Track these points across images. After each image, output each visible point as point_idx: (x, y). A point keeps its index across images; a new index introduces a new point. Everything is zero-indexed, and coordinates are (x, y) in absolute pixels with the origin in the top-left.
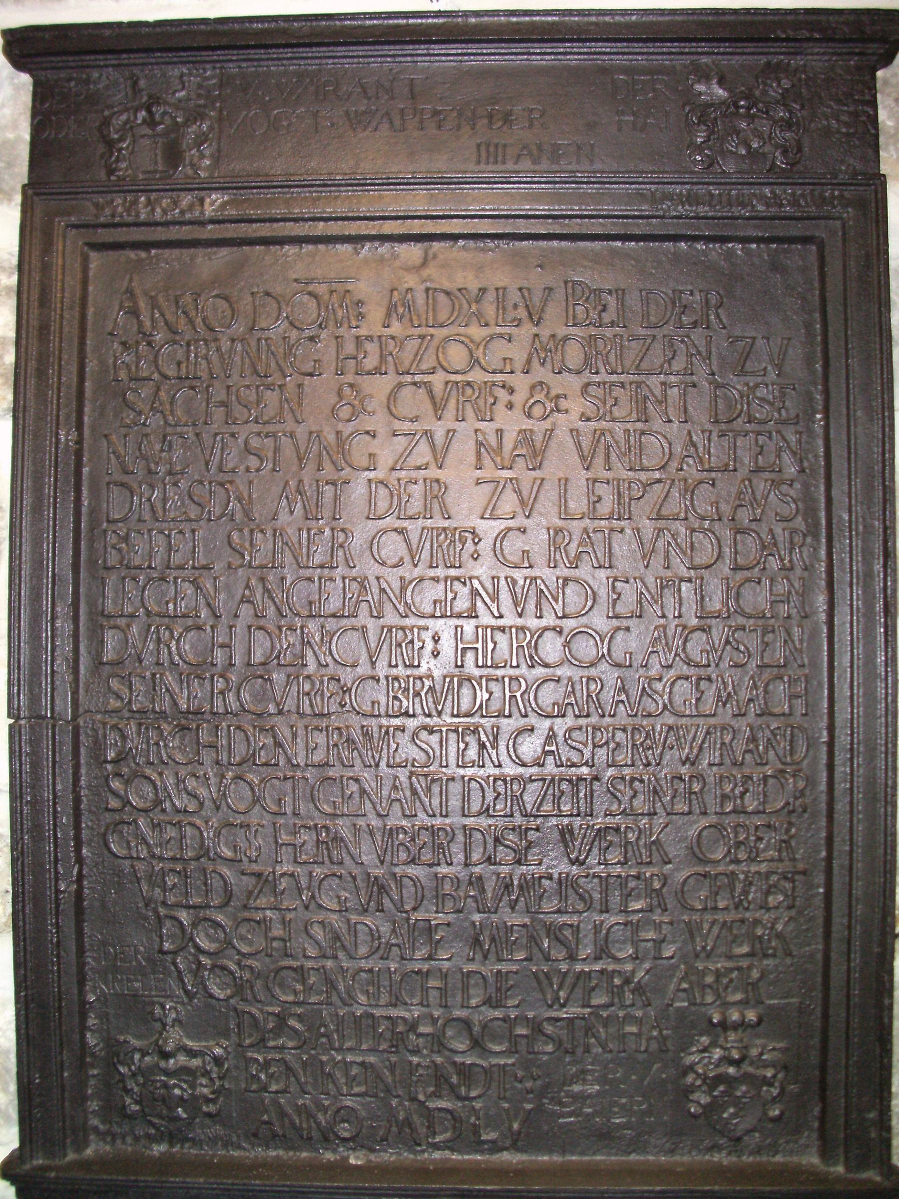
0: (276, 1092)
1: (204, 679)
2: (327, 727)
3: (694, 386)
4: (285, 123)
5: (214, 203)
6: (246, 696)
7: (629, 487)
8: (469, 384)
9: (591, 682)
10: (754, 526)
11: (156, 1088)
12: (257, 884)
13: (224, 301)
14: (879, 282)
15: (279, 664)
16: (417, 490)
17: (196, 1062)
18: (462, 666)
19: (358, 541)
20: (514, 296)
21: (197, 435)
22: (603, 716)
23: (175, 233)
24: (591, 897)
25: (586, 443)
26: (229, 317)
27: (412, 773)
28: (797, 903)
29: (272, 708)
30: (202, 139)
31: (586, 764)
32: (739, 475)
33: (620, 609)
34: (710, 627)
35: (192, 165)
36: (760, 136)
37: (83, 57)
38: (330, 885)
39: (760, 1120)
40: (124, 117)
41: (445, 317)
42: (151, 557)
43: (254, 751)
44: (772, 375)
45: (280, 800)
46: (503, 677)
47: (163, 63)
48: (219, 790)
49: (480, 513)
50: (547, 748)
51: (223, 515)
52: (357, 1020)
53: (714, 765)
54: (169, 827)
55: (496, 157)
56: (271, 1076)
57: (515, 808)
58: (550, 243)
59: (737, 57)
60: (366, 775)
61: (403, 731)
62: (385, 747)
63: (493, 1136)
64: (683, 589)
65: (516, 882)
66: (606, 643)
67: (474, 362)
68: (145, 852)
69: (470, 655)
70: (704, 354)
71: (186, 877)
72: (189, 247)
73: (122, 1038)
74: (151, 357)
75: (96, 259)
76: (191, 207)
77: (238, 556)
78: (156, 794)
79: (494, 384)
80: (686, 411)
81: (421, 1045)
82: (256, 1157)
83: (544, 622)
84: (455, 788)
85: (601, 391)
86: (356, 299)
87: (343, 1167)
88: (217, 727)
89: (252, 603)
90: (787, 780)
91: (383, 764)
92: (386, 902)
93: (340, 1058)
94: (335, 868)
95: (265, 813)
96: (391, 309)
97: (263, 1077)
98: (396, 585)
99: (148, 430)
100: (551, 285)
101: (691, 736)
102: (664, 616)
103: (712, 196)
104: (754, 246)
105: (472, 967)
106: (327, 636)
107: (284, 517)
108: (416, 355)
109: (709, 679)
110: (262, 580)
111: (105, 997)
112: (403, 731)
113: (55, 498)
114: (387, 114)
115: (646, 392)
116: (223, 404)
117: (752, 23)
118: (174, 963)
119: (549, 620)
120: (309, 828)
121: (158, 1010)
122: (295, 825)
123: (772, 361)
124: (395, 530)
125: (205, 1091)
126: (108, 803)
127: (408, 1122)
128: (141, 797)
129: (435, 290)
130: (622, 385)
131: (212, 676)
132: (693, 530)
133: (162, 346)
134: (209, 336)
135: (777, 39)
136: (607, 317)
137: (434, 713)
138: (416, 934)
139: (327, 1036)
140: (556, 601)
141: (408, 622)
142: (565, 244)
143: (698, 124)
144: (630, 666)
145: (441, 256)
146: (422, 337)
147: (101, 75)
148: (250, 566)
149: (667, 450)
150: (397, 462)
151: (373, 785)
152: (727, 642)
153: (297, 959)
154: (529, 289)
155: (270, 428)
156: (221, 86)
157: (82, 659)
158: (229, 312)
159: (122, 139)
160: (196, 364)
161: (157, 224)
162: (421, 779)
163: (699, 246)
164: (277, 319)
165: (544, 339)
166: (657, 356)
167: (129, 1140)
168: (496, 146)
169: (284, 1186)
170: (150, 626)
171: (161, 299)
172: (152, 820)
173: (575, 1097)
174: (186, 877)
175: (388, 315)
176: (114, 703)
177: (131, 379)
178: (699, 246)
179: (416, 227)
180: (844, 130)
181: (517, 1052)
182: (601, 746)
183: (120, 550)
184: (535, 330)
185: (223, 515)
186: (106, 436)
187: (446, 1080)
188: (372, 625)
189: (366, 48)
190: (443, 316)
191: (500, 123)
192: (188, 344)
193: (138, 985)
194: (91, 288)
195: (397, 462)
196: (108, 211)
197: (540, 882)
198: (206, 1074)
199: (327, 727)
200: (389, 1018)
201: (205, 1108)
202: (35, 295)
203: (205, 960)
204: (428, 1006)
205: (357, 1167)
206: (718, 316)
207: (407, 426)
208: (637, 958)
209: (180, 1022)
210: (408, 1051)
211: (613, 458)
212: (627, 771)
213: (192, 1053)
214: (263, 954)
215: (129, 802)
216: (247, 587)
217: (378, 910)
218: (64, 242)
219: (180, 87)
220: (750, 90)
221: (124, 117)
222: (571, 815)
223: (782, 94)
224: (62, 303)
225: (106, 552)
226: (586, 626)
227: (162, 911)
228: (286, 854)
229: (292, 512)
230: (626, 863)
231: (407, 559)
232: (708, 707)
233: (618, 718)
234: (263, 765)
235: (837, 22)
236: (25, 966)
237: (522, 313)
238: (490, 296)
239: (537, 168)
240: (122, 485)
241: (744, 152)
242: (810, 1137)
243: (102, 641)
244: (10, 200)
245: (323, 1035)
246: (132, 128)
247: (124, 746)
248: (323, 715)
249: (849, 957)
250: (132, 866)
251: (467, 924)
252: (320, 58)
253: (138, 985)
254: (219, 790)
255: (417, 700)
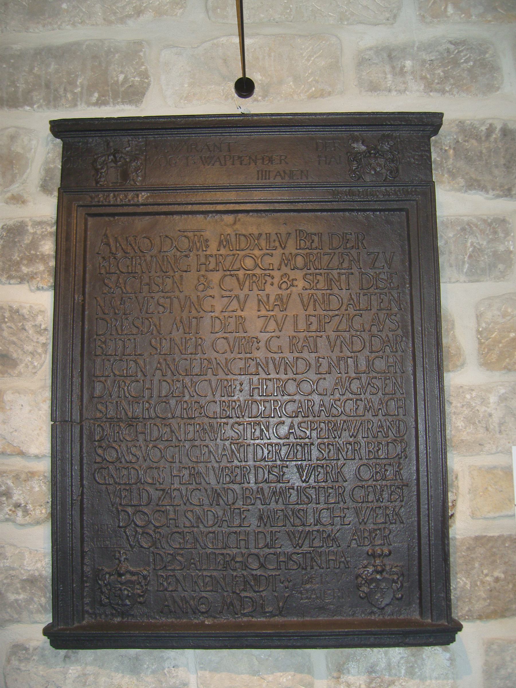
0: (172, 591)
1: (139, 403)
2: (194, 423)
3: (352, 274)
4: (174, 162)
5: (143, 197)
6: (158, 409)
7: (324, 318)
8: (254, 275)
9: (309, 402)
10: (379, 333)
11: (116, 591)
12: (163, 494)
13: (147, 240)
14: (433, 227)
15: (173, 396)
16: (232, 321)
17: (134, 578)
18: (253, 396)
19: (207, 344)
20: (274, 237)
21: (136, 297)
22: (315, 417)
23: (126, 210)
24: (312, 497)
25: (305, 300)
26: (150, 246)
27: (231, 443)
28: (405, 499)
29: (170, 415)
30: (136, 170)
31: (308, 438)
32: (373, 312)
33: (321, 370)
34: (361, 378)
35: (133, 180)
36: (380, 166)
37: (86, 133)
38: (196, 494)
39: (392, 599)
40: (103, 158)
41: (244, 246)
42: (116, 351)
43: (162, 435)
44: (386, 269)
45: (173, 456)
46: (271, 401)
47: (120, 136)
48: (146, 452)
49: (260, 330)
50: (291, 431)
51: (148, 332)
52: (208, 556)
53: (364, 437)
54: (123, 469)
55: (266, 176)
56: (169, 584)
57: (277, 457)
58: (289, 214)
59: (370, 132)
60: (212, 444)
61: (227, 424)
62: (219, 431)
63: (270, 609)
64: (349, 361)
65: (278, 490)
66: (315, 385)
67: (257, 265)
68: (112, 481)
69: (256, 391)
70: (357, 260)
71: (131, 492)
72: (133, 216)
73: (100, 568)
74: (116, 264)
75: (91, 221)
76: (133, 198)
77: (154, 350)
78: (118, 455)
79: (265, 275)
80: (349, 285)
81: (237, 567)
82: (162, 622)
83: (287, 377)
84: (251, 449)
85: (311, 277)
86: (205, 238)
87: (202, 625)
88: (145, 424)
89: (161, 370)
90: (397, 444)
91: (218, 440)
92: (221, 502)
93: (200, 574)
94: (198, 486)
95: (166, 462)
96: (220, 243)
97: (166, 584)
98: (224, 361)
99: (115, 295)
100: (290, 232)
101: (354, 425)
102: (340, 373)
103: (359, 192)
104: (378, 213)
105: (260, 530)
106: (194, 384)
107: (174, 333)
108: (231, 263)
109: (361, 400)
110: (165, 360)
111: (93, 549)
112: (227, 424)
113: (73, 325)
114: (218, 158)
115: (331, 276)
116: (148, 284)
117: (375, 118)
118: (125, 532)
119: (290, 375)
120: (186, 468)
121: (117, 555)
122: (180, 467)
123: (386, 262)
124: (223, 338)
125: (139, 591)
126: (96, 459)
127: (231, 603)
128: (110, 456)
129: (240, 235)
130: (321, 274)
131: (143, 402)
132: (353, 336)
133: (120, 259)
134: (141, 254)
135: (386, 125)
136: (314, 246)
137: (241, 416)
138: (234, 515)
139: (194, 564)
140: (293, 367)
141: (229, 377)
142: (295, 214)
143: (353, 161)
144: (326, 395)
145: (242, 220)
146: (234, 255)
147: (93, 141)
148: (160, 354)
149: (341, 302)
150: (223, 309)
151: (215, 448)
152: (369, 384)
153: (181, 528)
154: (280, 234)
155: (169, 294)
156: (146, 145)
157: (84, 395)
158: (150, 244)
159: (102, 168)
160: (136, 267)
161: (118, 206)
162: (236, 445)
163: (354, 214)
164: (171, 247)
165: (287, 255)
166: (336, 262)
167: (103, 616)
168: (266, 171)
169: (175, 633)
170: (115, 381)
171: (119, 239)
172: (116, 467)
173: (307, 590)
174: (131, 492)
175: (219, 245)
176: (99, 415)
177: (107, 273)
178: (354, 214)
179: (231, 207)
180: (417, 163)
181: (280, 569)
182: (314, 430)
183: (102, 348)
184: (282, 251)
185: (148, 332)
186: (96, 298)
187: (249, 583)
188: (214, 379)
189: (209, 129)
190: (243, 246)
191: (267, 162)
192: (132, 258)
193: (108, 542)
194: (89, 233)
195: (223, 309)
196: (96, 200)
197: (289, 491)
198: (139, 583)
199: (194, 423)
200: (223, 554)
201: (139, 600)
202: (64, 235)
203: (139, 530)
204: (240, 548)
205: (208, 625)
206: (362, 243)
207: (228, 293)
208: (333, 525)
209: (127, 559)
210: (232, 570)
211: (317, 305)
212: (325, 440)
213: (133, 574)
214: (166, 526)
215: (105, 459)
216: (159, 363)
217: (217, 505)
218: (77, 213)
219: (128, 146)
220: (376, 146)
221: (103, 158)
222: (302, 460)
223: (389, 148)
224: (76, 239)
225: (96, 349)
226: (307, 378)
227: (120, 508)
228: (177, 480)
229: (178, 330)
230: (327, 482)
231: (228, 350)
232: (361, 411)
233: (321, 417)
234: (166, 441)
235: (412, 118)
236: (57, 534)
237: (277, 244)
238: (264, 236)
239: (284, 181)
240: (103, 319)
241: (373, 173)
242: (415, 606)
243: (94, 388)
244: (51, 194)
245: (193, 563)
246: (107, 163)
247: (103, 434)
248: (193, 418)
249: (429, 522)
250: (106, 488)
251: (256, 510)
252: (189, 134)
253: (108, 542)
254: (146, 452)
255: (233, 410)
